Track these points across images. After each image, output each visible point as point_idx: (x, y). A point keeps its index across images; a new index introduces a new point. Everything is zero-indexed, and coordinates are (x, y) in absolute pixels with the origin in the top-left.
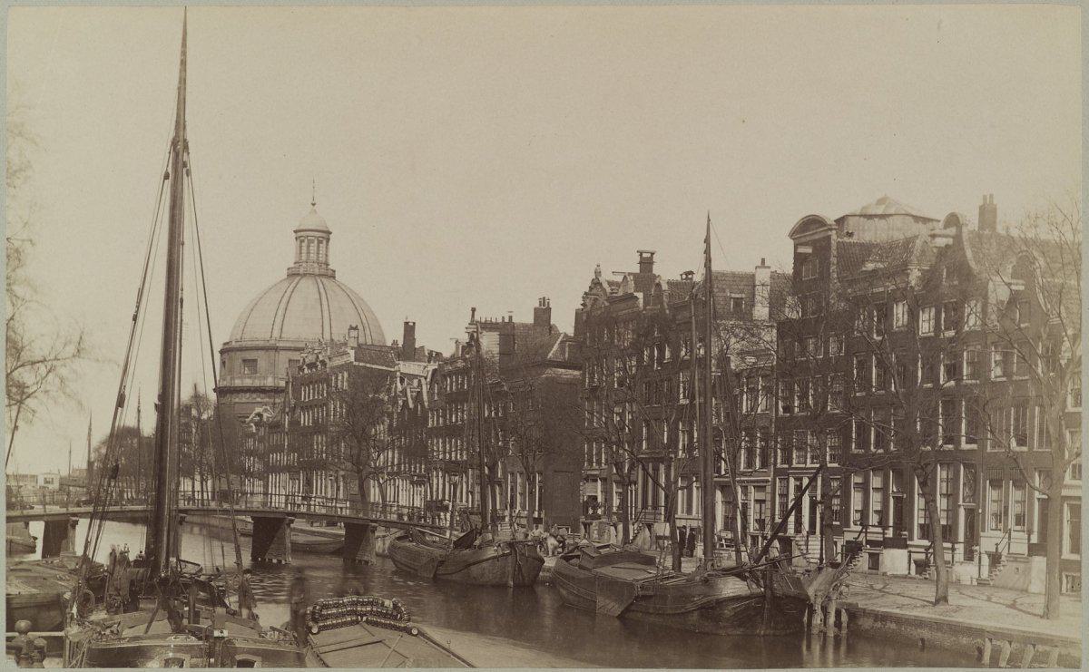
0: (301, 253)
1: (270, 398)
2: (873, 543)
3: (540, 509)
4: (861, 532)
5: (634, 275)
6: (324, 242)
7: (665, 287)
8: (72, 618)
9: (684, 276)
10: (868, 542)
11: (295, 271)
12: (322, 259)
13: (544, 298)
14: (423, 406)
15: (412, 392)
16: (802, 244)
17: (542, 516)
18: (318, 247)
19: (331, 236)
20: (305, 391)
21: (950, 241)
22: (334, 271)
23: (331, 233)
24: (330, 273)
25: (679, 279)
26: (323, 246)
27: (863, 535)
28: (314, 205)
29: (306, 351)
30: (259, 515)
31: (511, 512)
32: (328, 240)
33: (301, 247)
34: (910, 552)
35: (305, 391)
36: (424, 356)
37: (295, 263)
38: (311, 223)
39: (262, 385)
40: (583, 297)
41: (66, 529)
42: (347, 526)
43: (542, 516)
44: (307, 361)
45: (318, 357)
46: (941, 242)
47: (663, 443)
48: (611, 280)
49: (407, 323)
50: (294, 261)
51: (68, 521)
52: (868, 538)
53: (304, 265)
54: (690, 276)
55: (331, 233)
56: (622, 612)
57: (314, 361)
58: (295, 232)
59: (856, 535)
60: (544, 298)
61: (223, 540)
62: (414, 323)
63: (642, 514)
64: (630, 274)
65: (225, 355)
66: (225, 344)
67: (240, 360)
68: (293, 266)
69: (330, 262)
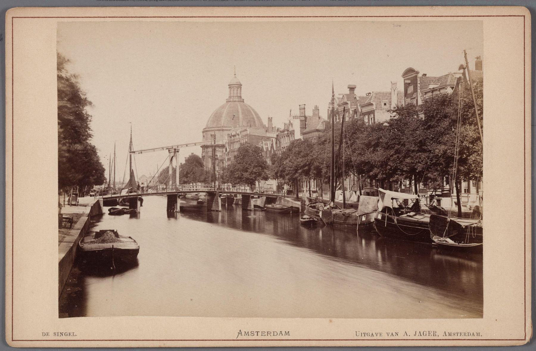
2: (438, 195)
4: (433, 191)
5: (347, 95)
6: (240, 88)
7: (358, 99)
8: (237, 204)
9: (367, 94)
10: (436, 195)
11: (229, 100)
12: (239, 95)
14: (273, 149)
17: (318, 190)
18: (237, 90)
19: (242, 86)
22: (243, 99)
26: (239, 90)
27: (434, 192)
28: (235, 75)
29: (232, 130)
33: (231, 91)
38: (234, 82)
42: (242, 196)
43: (318, 190)
44: (233, 134)
47: (186, 203)
50: (228, 96)
51: (137, 197)
52: (436, 194)
53: (232, 97)
58: (229, 85)
59: (431, 192)
60: (316, 106)
61: (82, 230)
64: (345, 94)
68: (228, 98)
69: (242, 96)
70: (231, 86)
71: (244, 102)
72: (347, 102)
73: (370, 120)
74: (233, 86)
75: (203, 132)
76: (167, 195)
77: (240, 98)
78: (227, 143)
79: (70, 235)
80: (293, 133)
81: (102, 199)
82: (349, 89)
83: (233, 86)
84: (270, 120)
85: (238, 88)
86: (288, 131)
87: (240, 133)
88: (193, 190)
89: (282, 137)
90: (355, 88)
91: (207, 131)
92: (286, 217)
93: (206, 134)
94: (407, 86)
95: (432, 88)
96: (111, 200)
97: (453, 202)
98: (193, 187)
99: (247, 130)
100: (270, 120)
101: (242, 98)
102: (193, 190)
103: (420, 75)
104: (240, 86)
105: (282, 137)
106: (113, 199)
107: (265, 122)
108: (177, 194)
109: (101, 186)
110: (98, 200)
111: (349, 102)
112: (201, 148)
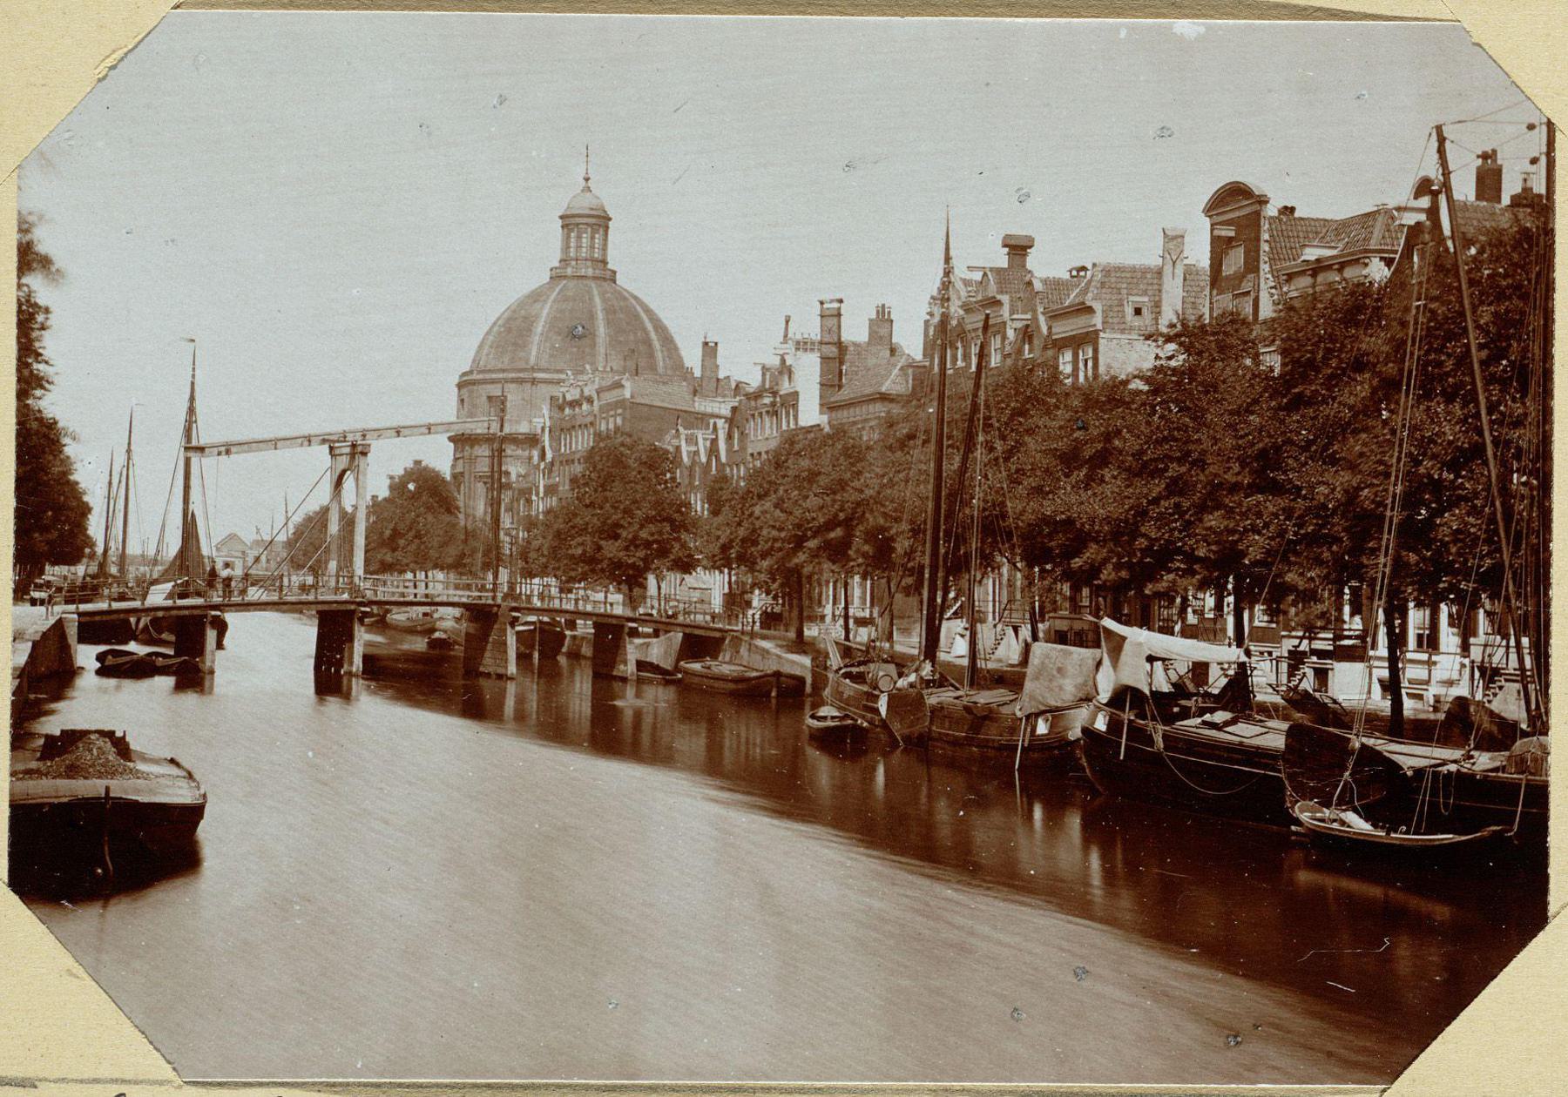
0: (568, 247)
1: (523, 450)
2: (1321, 654)
3: (872, 604)
7: (1038, 286)
9: (1074, 273)
10: (1314, 652)
13: (883, 306)
14: (718, 458)
15: (705, 439)
16: (1216, 224)
20: (565, 440)
21: (1422, 217)
22: (614, 272)
23: (610, 219)
25: (1067, 276)
28: (587, 180)
29: (567, 384)
30: (326, 607)
31: (834, 609)
32: (607, 228)
34: (1370, 668)
35: (565, 440)
36: (730, 389)
37: (560, 261)
38: (584, 204)
39: (513, 431)
40: (930, 304)
41: (352, 621)
42: (596, 625)
45: (582, 391)
46: (1410, 219)
48: (968, 278)
49: (706, 344)
52: (1313, 647)
53: (573, 263)
54: (1082, 273)
55: (610, 219)
56: (708, 737)
57: (578, 397)
59: (1296, 642)
60: (883, 306)
62: (716, 344)
63: (1006, 612)
64: (991, 269)
65: (464, 391)
66: (464, 374)
67: (484, 398)
68: (557, 265)
70: (572, 220)
72: (999, 297)
73: (1081, 365)
75: (460, 386)
80: (791, 401)
81: (76, 616)
82: (1007, 249)
84: (710, 350)
85: (594, 232)
86: (775, 394)
87: (598, 393)
88: (415, 595)
90: (1030, 247)
91: (473, 383)
93: (471, 392)
94: (1220, 247)
95: (1313, 258)
97: (1375, 680)
99: (623, 386)
100: (710, 350)
101: (609, 266)
102: (415, 595)
103: (1271, 210)
104: (601, 221)
107: (692, 358)
108: (353, 607)
110: (61, 618)
111: (1005, 299)
112: (452, 445)
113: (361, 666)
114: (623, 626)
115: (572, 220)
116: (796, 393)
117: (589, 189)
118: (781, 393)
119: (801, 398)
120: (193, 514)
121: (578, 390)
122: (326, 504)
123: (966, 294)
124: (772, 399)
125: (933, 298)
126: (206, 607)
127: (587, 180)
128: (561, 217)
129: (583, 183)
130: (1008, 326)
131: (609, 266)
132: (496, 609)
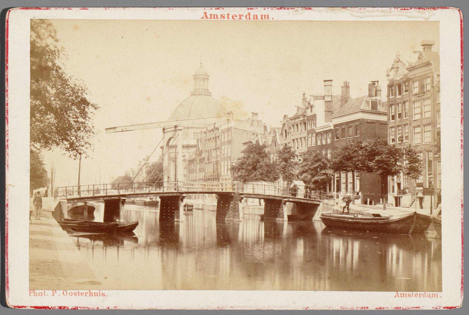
22: (210, 93)
24: (209, 94)
28: (201, 64)
32: (208, 79)
37: (194, 90)
44: (209, 129)
45: (207, 128)
55: (209, 76)
68: (193, 91)
70: (196, 77)
71: (211, 96)
74: (200, 76)
76: (105, 200)
77: (207, 91)
78: (199, 141)
79: (52, 179)
81: (66, 201)
83: (200, 76)
85: (204, 80)
86: (304, 116)
88: (222, 189)
89: (293, 126)
90: (433, 45)
92: (341, 238)
96: (167, 197)
98: (222, 186)
101: (209, 91)
102: (222, 189)
104: (206, 78)
105: (293, 126)
106: (113, 198)
108: (179, 194)
109: (250, 11)
110: (60, 202)
113: (414, 262)
114: (282, 200)
115: (196, 77)
116: (315, 115)
117: (201, 67)
118: (307, 116)
119: (317, 115)
120: (449, 8)
121: (205, 128)
122: (154, 159)
123: (408, 65)
124: (303, 118)
125: (342, 87)
126: (119, 196)
127: (201, 64)
128: (194, 76)
129: (200, 65)
130: (434, 73)
131: (209, 91)
132: (233, 194)
